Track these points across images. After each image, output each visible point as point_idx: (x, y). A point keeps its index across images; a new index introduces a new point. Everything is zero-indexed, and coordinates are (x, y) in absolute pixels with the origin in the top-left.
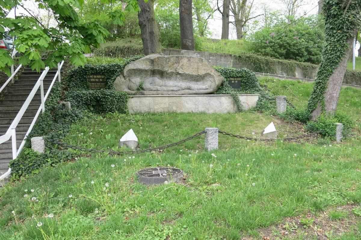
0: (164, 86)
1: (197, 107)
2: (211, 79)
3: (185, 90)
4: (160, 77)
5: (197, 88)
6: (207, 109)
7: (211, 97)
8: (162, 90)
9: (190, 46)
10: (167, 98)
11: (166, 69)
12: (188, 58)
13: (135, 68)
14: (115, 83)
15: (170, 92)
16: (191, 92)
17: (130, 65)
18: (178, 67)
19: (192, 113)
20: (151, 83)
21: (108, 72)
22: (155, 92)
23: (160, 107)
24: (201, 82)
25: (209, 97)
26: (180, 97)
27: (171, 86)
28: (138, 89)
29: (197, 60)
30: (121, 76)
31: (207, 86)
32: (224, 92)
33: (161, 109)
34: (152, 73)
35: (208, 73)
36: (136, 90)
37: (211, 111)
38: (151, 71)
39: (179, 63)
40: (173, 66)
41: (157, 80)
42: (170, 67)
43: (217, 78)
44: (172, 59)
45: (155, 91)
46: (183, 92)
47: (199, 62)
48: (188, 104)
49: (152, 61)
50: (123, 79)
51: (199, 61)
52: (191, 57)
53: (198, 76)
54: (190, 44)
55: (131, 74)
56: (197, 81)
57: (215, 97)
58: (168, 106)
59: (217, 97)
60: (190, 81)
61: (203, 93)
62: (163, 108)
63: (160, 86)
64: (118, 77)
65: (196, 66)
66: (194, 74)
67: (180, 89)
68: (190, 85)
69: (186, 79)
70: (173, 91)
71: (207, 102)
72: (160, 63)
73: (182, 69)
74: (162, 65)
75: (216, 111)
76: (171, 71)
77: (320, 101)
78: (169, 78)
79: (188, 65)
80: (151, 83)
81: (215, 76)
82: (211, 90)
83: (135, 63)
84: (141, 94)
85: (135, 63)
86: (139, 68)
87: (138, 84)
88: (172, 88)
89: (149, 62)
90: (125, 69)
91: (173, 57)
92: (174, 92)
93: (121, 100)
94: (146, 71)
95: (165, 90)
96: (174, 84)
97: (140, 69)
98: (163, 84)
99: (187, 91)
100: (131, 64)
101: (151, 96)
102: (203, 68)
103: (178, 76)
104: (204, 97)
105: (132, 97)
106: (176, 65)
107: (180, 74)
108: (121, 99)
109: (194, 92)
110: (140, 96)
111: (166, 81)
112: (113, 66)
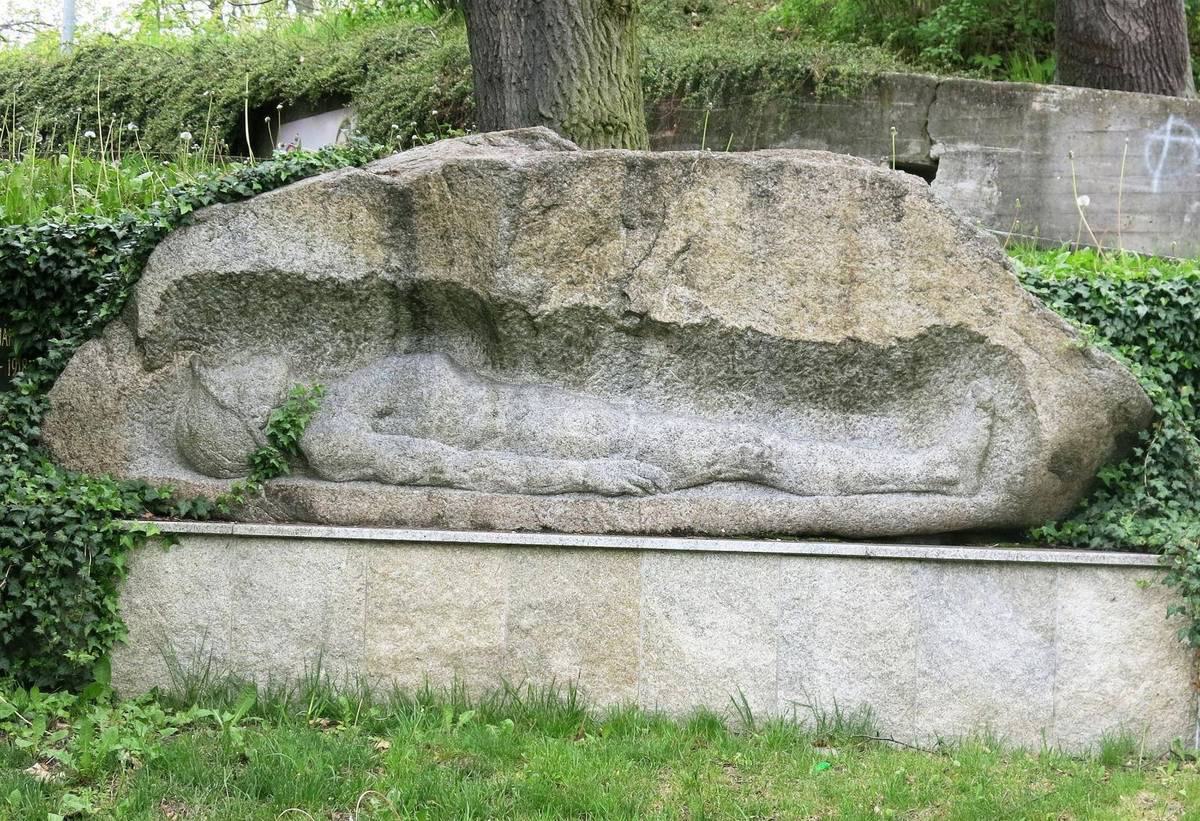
0: (507, 442)
1: (793, 664)
2: (987, 387)
3: (709, 493)
4: (479, 357)
5: (832, 470)
6: (900, 691)
7: (949, 575)
8: (478, 479)
9: (1138, 49)
10: (497, 557)
11: (517, 281)
12: (749, 175)
13: (238, 267)
14: (53, 397)
15: (557, 508)
16: (764, 507)
17: (198, 235)
18: (650, 268)
19: (732, 722)
20: (382, 414)
21: (39, 294)
22: (411, 501)
23: (422, 647)
24: (895, 419)
25: (926, 575)
26: (628, 562)
27: (567, 449)
28: (261, 467)
29: (838, 203)
30: (117, 333)
31: (940, 453)
32: (1126, 527)
33: (432, 665)
34: (405, 314)
35: (959, 329)
36: (237, 472)
37: (942, 718)
38: (393, 292)
39: (653, 220)
40: (593, 251)
41: (447, 383)
42: (561, 257)
43: (1053, 383)
44: (583, 190)
45: (412, 483)
46: (683, 508)
47: (861, 218)
48: (700, 631)
49: (401, 208)
50: (128, 369)
51: (864, 204)
52: (780, 167)
53: (849, 353)
54: (1139, 32)
55: (212, 319)
56: (847, 407)
57: (991, 576)
58: (500, 638)
59: (1009, 575)
60: (780, 400)
61: (892, 525)
62: (455, 660)
63: (472, 445)
64: (93, 347)
65: (826, 258)
66: (815, 329)
67: (665, 478)
68: (770, 438)
69: (734, 382)
70: (585, 490)
71: (904, 626)
72: (460, 220)
73: (689, 284)
74: (481, 245)
75: (1000, 723)
76: (576, 298)
77: (1016, 687)
78: (566, 364)
79: (743, 242)
80: (382, 414)
81: (1028, 357)
82: (986, 501)
83: (246, 222)
84: (279, 509)
85: (246, 218)
86: (282, 265)
87: (262, 411)
88: (576, 469)
89: (372, 208)
90: (147, 277)
91: (590, 162)
92: (594, 505)
93: (53, 559)
94: (342, 292)
95: (514, 481)
96: (599, 428)
97: (284, 277)
98: (501, 423)
99: (729, 501)
100: (203, 232)
101: (366, 533)
102: (901, 278)
103: (654, 350)
104: (875, 569)
105: (171, 538)
106: (621, 246)
107: (664, 330)
108: (52, 545)
109: (801, 510)
110: (289, 530)
111: (534, 399)
112: (89, 244)
